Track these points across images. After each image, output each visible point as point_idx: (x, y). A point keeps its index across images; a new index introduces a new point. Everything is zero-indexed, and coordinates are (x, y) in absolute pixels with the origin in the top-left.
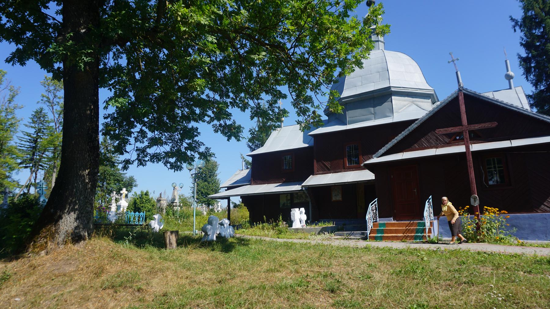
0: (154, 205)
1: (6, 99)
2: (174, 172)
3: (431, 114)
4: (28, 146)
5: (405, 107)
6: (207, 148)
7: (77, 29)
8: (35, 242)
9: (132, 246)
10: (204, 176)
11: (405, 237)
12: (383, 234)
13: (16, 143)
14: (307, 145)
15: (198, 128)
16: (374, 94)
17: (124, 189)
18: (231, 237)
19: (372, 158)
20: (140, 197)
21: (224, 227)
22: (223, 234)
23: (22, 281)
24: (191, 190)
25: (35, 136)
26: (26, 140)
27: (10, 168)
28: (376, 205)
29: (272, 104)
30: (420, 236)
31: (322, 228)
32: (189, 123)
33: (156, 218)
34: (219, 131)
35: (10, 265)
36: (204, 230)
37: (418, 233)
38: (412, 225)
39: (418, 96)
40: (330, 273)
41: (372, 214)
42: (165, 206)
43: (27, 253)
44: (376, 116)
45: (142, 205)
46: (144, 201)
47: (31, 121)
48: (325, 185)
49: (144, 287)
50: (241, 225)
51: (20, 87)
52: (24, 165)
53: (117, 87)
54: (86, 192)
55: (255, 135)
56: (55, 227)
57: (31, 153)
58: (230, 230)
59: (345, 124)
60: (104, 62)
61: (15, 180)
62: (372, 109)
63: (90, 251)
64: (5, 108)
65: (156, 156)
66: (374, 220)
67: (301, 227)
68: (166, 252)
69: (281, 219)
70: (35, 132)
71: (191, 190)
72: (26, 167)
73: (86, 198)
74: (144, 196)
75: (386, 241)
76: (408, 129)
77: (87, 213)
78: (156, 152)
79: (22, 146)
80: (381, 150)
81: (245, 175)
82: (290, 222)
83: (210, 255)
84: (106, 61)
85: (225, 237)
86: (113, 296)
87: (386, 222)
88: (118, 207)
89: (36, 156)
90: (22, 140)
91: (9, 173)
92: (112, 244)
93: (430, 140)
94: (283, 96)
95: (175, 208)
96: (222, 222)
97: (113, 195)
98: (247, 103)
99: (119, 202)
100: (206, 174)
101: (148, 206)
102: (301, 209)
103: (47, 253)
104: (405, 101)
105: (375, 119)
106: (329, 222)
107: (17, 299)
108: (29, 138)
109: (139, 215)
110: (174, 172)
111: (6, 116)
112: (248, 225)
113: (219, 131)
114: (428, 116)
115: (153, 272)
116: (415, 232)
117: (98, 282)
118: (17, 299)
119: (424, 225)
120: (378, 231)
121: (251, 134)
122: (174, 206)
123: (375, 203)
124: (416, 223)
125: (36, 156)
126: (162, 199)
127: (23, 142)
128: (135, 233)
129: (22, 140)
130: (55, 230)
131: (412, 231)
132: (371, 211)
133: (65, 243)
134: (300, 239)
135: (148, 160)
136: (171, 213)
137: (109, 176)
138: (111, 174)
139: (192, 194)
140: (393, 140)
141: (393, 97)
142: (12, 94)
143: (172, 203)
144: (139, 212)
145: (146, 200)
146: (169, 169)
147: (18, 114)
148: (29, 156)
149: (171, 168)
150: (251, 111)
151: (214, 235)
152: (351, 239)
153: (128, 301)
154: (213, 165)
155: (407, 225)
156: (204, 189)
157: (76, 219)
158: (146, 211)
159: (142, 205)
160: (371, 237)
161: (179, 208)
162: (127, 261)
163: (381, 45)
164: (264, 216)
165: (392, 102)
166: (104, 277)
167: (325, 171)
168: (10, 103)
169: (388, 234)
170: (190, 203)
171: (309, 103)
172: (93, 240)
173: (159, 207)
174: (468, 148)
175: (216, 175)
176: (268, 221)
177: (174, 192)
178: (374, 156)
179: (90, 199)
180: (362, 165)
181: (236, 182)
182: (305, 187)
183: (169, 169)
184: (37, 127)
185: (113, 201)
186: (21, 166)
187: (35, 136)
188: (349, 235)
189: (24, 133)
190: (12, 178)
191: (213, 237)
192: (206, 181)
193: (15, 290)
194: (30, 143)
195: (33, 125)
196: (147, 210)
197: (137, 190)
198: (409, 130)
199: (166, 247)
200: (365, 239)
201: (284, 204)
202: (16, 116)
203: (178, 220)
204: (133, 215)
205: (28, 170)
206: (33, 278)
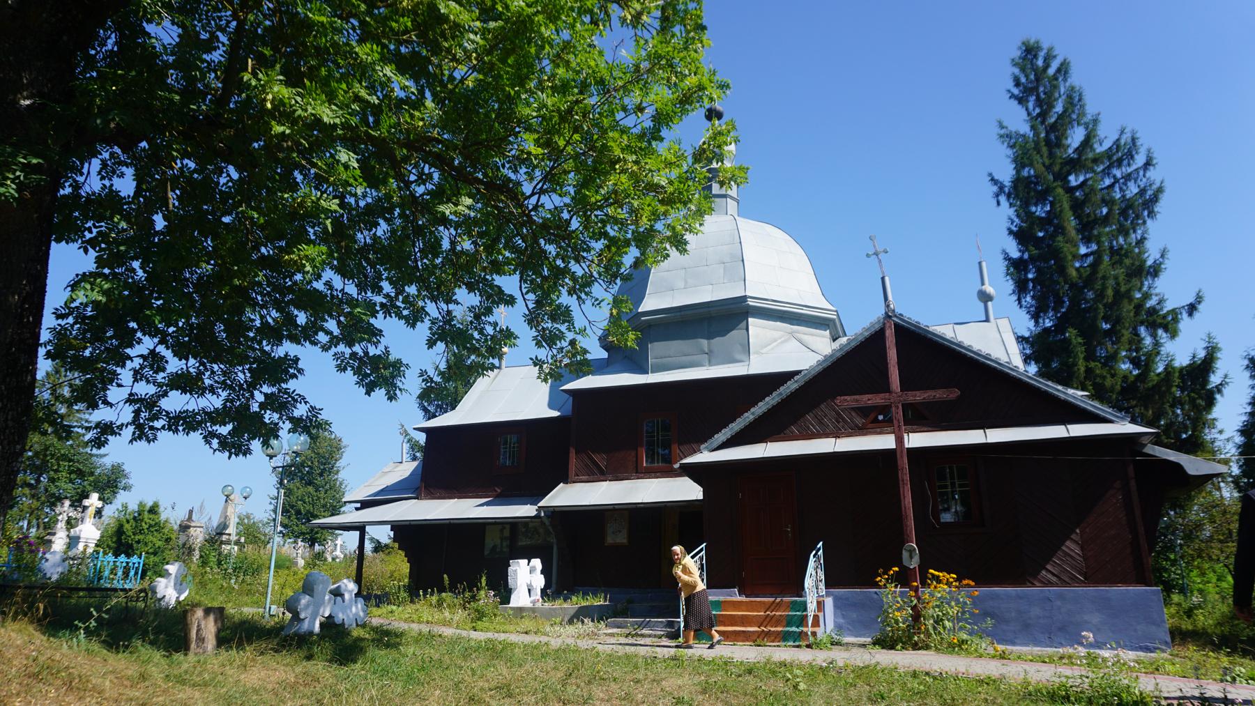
0: (170, 539)
2: (229, 458)
3: (828, 363)
5: (775, 344)
9: (95, 646)
10: (308, 472)
14: (555, 414)
15: (298, 359)
16: (711, 309)
19: (698, 451)
20: (135, 518)
21: (344, 601)
22: (340, 617)
24: (271, 503)
28: (701, 559)
29: (479, 314)
32: (277, 345)
33: (170, 572)
34: (349, 369)
38: (777, 606)
42: (198, 541)
45: (137, 538)
46: (145, 527)
59: (644, 371)
60: (75, 181)
62: (704, 342)
65: (184, 419)
68: (186, 662)
71: (271, 503)
78: (185, 409)
80: (720, 434)
81: (407, 474)
82: (504, 593)
83: (298, 669)
84: (81, 179)
85: (343, 624)
87: (722, 598)
88: (73, 541)
92: (40, 639)
97: (62, 510)
98: (423, 308)
101: (155, 540)
102: (533, 560)
104: (774, 330)
106: (595, 594)
109: (127, 563)
110: (229, 458)
112: (403, 594)
116: (785, 622)
121: (423, 381)
122: (222, 543)
123: (701, 554)
126: (193, 524)
131: (778, 621)
134: (526, 633)
135: (163, 427)
136: (213, 559)
137: (57, 460)
138: (62, 455)
140: (746, 414)
143: (217, 534)
144: (128, 556)
145: (151, 526)
150: (430, 329)
151: (315, 620)
155: (770, 607)
156: (305, 503)
158: (147, 553)
159: (137, 538)
161: (236, 548)
163: (732, 205)
164: (445, 576)
165: (747, 329)
169: (725, 626)
170: (265, 535)
174: (900, 441)
176: (453, 588)
177: (225, 509)
178: (702, 446)
180: (676, 466)
181: (382, 490)
182: (545, 509)
183: (215, 451)
185: (61, 525)
188: (641, 626)
192: (310, 483)
196: (151, 551)
197: (128, 500)
198: (781, 394)
201: (495, 547)
204: (111, 564)
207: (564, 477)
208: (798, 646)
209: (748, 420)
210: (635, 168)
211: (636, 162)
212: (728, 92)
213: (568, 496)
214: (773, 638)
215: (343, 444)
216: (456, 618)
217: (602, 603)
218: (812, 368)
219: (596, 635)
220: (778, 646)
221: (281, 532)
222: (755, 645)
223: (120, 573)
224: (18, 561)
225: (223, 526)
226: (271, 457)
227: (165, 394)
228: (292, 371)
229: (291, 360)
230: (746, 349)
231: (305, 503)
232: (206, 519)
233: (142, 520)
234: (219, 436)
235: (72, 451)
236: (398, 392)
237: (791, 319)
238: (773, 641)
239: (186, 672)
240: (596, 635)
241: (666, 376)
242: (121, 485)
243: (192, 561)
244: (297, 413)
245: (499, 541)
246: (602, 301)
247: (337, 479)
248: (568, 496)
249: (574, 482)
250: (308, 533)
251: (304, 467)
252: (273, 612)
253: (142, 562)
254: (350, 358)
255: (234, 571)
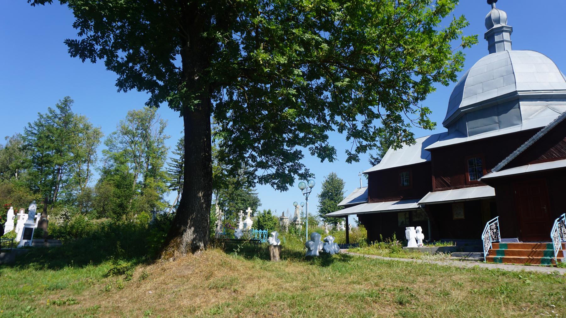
0: (276, 223)
1: (158, 132)
2: (281, 192)
3: (561, 120)
4: (176, 171)
5: (537, 113)
6: (306, 170)
7: (192, 77)
8: (166, 250)
9: (242, 258)
10: (331, 195)
11: (530, 261)
12: (505, 255)
13: (166, 168)
14: (424, 160)
15: (301, 151)
16: (497, 101)
17: (249, 208)
18: (335, 253)
19: (491, 172)
20: (263, 216)
21: (329, 244)
22: (328, 250)
23: (155, 280)
24: (318, 208)
25: (181, 161)
26: (173, 165)
27: (162, 191)
28: (496, 224)
29: (366, 124)
30: (548, 259)
31: (439, 248)
32: (293, 147)
33: (273, 235)
34: (316, 153)
35: (148, 268)
36: (307, 246)
37: (547, 256)
38: (539, 247)
39: (554, 98)
40: (406, 287)
41: (490, 233)
42: (287, 224)
43: (161, 259)
44: (501, 125)
45: (264, 223)
46: (267, 219)
47: (177, 149)
48: (444, 202)
49: (240, 290)
50: (358, 244)
51: (167, 120)
52: (173, 188)
53: (224, 121)
54: (202, 210)
55: (352, 155)
56: (180, 239)
57: (178, 177)
58: (334, 247)
59: (465, 136)
60: (220, 98)
61: (167, 201)
62: (496, 118)
63: (205, 260)
64: (157, 139)
65: (264, 178)
66: (493, 240)
67: (417, 247)
68: (268, 263)
69: (395, 238)
70: (181, 158)
71: (318, 208)
72: (174, 190)
73: (202, 215)
74: (267, 215)
75: (506, 263)
76: (532, 138)
77: (204, 228)
78: (264, 174)
79: (171, 170)
80: (501, 163)
81: (363, 193)
82: (404, 241)
83: (306, 267)
84: (221, 97)
85: (329, 253)
86: (215, 294)
87: (509, 243)
88: (245, 225)
89: (182, 179)
90: (171, 166)
91: (162, 195)
92: (224, 254)
93: (561, 150)
94: (376, 116)
95: (298, 227)
96: (326, 239)
97: (240, 214)
98: (344, 124)
99: (245, 221)
100: (332, 193)
101: (270, 224)
102: (417, 227)
103: (174, 260)
104: (536, 105)
105: (500, 128)
106: (447, 242)
107: (150, 292)
108: (176, 163)
109: (262, 233)
110: (281, 192)
111: (158, 146)
112: (365, 243)
113: (316, 153)
114: (556, 123)
115: (250, 278)
116: (543, 254)
117: (206, 284)
118: (150, 292)
119: (551, 246)
120: (498, 253)
121: (348, 154)
122: (296, 224)
123: (496, 222)
124: (545, 244)
125: (182, 179)
126: (284, 218)
127: (171, 168)
128: (242, 246)
129: (171, 166)
130: (180, 241)
131: (539, 254)
132: (489, 231)
133: (187, 252)
134: (412, 258)
135: (257, 182)
136: (293, 231)
137: (237, 196)
138: (238, 194)
139: (319, 213)
140: (515, 152)
141: (520, 103)
142: (161, 126)
143: (294, 221)
144: (262, 230)
145: (268, 219)
146: (276, 190)
147: (167, 143)
148: (176, 180)
149: (278, 189)
150: (348, 132)
151: (316, 250)
152: (468, 260)
153: (225, 299)
154: (339, 183)
155: (534, 247)
156: (331, 208)
157: (194, 232)
158: (268, 229)
159: (264, 223)
160: (487, 259)
161: (301, 226)
162: (233, 269)
163: (507, 45)
164: (381, 235)
165: (519, 108)
166: (211, 280)
167: (444, 187)
168: (160, 134)
169: (509, 255)
170: (316, 221)
171: (400, 122)
172: (208, 250)
173: (282, 226)
175: (343, 194)
176: (384, 240)
177: (296, 211)
178: (492, 170)
179: (205, 216)
180: (479, 180)
181: (353, 200)
182: (422, 204)
183: (276, 190)
184: (182, 153)
185: (241, 220)
186: (171, 188)
187: (181, 161)
188: (468, 256)
189: (172, 159)
190: (164, 199)
191: (316, 252)
192: (332, 199)
193: (150, 286)
194: (177, 168)
195: (179, 152)
196: (270, 228)
197: (261, 209)
198: (534, 139)
199: (270, 259)
200: (482, 260)
201: (403, 222)
202: (165, 145)
203: (300, 238)
204: (257, 233)
205: (176, 192)
206: (162, 278)
207: (430, 189)
208: (549, 266)
209: (516, 154)
210: (413, 51)
211: (412, 48)
212: (458, 3)
213: (432, 197)
214: (536, 262)
215: (343, 182)
216: (384, 252)
217: (451, 246)
218: (551, 124)
219: (445, 259)
220: (538, 266)
221: (323, 220)
222: (525, 265)
223: (260, 236)
224: (227, 232)
225: (296, 218)
226: (302, 190)
227: (256, 170)
228: (299, 156)
229: (298, 152)
230: (520, 118)
231: (331, 208)
232: (290, 216)
233: (265, 217)
234: (276, 184)
235: (241, 193)
236: (333, 160)
237: (546, 98)
238: (536, 264)
239: (268, 266)
240: (445, 259)
241: (477, 137)
242: (258, 204)
243: (285, 232)
244: (300, 172)
245: (404, 219)
246: (416, 111)
247: (343, 197)
248: (432, 197)
249: (436, 191)
250: (334, 220)
251: (329, 193)
252: (300, 249)
253: (267, 232)
254: (315, 149)
255: (301, 235)
